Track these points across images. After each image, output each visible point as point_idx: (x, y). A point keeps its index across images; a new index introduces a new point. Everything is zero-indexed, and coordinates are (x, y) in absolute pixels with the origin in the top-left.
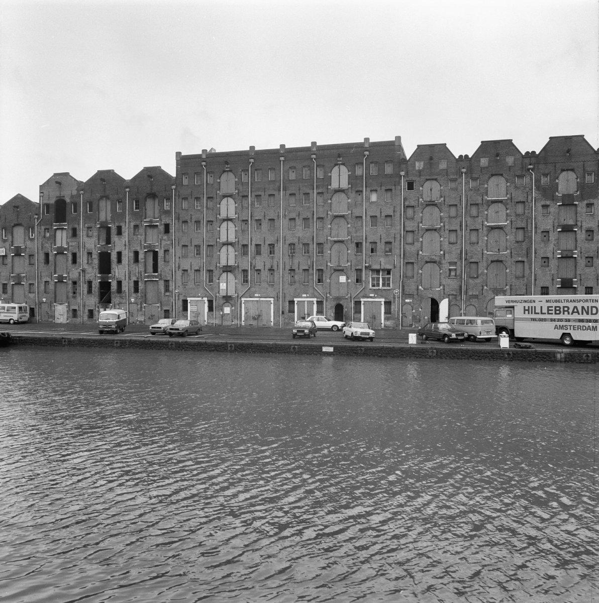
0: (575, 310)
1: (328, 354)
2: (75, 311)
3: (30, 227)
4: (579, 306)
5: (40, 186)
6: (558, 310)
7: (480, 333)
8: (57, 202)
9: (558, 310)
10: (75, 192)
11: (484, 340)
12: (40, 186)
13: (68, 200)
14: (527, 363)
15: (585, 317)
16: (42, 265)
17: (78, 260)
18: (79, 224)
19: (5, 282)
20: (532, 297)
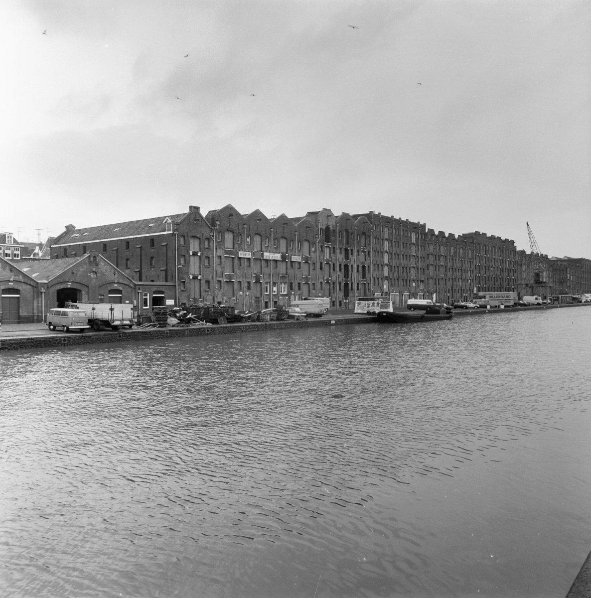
0: (504, 297)
1: (333, 325)
2: (334, 301)
3: (312, 244)
4: (505, 295)
5: (512, 242)
6: (499, 297)
7: (72, 324)
8: (326, 228)
9: (499, 297)
10: (334, 224)
11: (79, 330)
12: (512, 242)
13: (331, 229)
14: (24, 351)
15: (507, 298)
16: (319, 270)
17: (336, 269)
18: (336, 246)
19: (300, 282)
20: (492, 293)
